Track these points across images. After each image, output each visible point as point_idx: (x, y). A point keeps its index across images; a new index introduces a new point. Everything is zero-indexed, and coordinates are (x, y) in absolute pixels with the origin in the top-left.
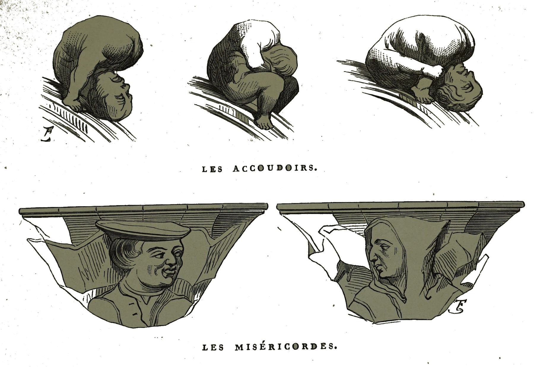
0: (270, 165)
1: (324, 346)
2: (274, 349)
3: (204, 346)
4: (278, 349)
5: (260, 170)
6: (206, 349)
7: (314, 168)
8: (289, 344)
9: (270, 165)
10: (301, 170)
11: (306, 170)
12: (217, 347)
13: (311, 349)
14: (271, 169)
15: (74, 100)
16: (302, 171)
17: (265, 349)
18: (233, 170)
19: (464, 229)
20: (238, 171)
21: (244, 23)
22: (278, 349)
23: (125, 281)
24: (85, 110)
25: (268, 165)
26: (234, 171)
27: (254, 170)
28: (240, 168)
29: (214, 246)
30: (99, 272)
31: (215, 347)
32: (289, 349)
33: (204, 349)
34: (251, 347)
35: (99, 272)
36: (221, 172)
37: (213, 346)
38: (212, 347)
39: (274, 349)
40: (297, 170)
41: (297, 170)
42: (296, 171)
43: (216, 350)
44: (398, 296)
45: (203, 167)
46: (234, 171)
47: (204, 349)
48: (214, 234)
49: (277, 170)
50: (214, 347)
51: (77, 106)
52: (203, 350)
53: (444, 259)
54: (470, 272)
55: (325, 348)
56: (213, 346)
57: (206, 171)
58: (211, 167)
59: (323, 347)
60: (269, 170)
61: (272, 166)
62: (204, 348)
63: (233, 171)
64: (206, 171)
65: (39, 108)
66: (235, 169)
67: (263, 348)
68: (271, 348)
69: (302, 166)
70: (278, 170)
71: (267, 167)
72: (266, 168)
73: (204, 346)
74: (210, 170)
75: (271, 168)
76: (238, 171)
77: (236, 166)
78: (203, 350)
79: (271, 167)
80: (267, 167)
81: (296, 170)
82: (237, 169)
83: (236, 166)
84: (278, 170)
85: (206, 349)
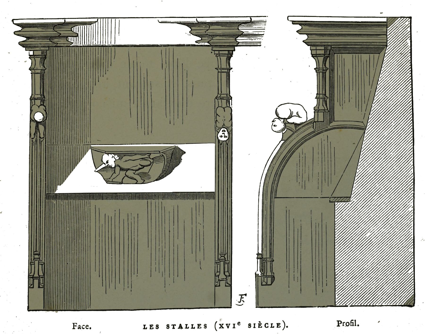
1: (260, 325)
3: (144, 325)
4: (233, 328)
6: (187, 327)
8: (268, 324)
12: (154, 327)
15: (108, 156)
17: (201, 328)
20: (227, 324)
21: (330, 199)
22: (233, 328)
24: (105, 157)
27: (268, 327)
31: (153, 326)
33: (144, 328)
34: (252, 326)
37: (199, 325)
43: (153, 328)
46: (229, 324)
47: (144, 328)
51: (150, 179)
52: (143, 329)
53: (159, 161)
54: (172, 171)
59: (260, 326)
62: (186, 326)
73: (144, 325)
78: (143, 329)
85: (187, 327)
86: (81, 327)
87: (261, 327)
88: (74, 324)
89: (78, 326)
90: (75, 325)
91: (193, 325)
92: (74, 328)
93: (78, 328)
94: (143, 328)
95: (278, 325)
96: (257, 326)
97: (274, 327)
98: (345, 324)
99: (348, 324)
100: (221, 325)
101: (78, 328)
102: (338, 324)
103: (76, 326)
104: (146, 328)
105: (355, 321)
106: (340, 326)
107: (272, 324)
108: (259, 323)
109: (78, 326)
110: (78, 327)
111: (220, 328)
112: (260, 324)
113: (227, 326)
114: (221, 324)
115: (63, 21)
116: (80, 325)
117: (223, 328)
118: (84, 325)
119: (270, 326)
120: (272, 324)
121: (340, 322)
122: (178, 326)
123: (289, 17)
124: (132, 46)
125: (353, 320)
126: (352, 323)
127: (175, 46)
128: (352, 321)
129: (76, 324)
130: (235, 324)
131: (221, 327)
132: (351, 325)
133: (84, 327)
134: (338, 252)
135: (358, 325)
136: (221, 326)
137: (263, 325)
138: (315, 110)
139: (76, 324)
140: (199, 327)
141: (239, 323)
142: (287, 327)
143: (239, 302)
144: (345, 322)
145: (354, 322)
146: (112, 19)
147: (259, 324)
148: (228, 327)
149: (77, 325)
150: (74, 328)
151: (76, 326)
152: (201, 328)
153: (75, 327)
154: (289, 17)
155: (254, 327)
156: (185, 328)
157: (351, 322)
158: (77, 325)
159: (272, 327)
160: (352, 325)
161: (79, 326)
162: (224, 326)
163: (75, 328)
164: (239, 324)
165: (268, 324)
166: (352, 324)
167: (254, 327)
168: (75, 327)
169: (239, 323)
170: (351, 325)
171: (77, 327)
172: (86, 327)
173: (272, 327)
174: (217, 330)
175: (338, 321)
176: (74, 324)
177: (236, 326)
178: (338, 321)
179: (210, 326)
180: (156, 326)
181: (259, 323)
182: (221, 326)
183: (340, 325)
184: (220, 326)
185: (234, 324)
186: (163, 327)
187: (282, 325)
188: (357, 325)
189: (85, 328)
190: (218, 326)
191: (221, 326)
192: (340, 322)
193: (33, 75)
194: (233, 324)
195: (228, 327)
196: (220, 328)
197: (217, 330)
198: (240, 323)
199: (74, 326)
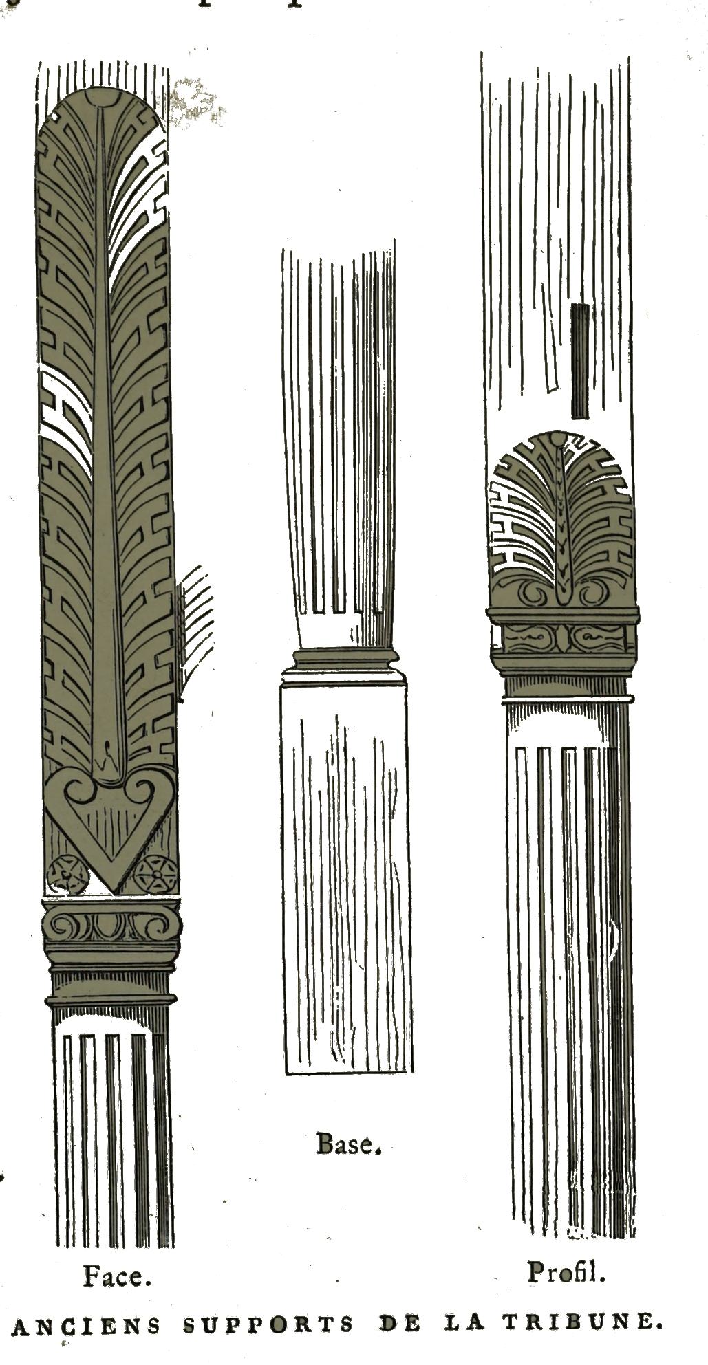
0: (595, 1315)
3: (450, 1317)
5: (277, 1329)
7: (653, 1321)
9: (595, 1315)
11: (310, 1331)
14: (210, 1327)
16: (87, 1336)
19: (112, 86)
20: (25, 1334)
23: (81, 781)
25: (202, 1319)
26: (14, 1334)
27: (73, 1333)
28: (31, 1327)
30: (352, 630)
33: (450, 1328)
34: (545, 1322)
35: (352, 630)
36: (348, 1331)
41: (513, 1328)
42: (87, 1336)
44: (344, 1028)
45: (551, 1315)
46: (14, 1334)
47: (450, 1328)
55: (114, 1332)
57: (457, 1328)
58: (639, 1314)
59: (644, 1322)
60: (593, 1326)
61: (602, 1315)
63: (468, 1329)
64: (457, 1328)
65: (124, 1247)
66: (472, 1323)
69: (529, 1316)
70: (384, 1328)
71: (202, 1324)
72: (585, 1321)
75: (597, 1323)
76: (25, 1334)
77: (475, 1316)
79: (210, 1324)
80: (589, 1318)
82: (22, 1328)
83: (475, 1316)
84: (384, 1328)
85: (454, 1326)
86: (114, 1281)
88: (88, 1268)
89: (104, 1277)
90: (93, 1271)
92: (88, 1284)
93: (104, 1284)
94: (84, 1331)
98: (556, 1276)
99: (566, 1276)
101: (104, 1284)
103: (96, 1275)
105: (592, 1262)
109: (104, 1277)
110: (103, 1279)
114: (21, 1335)
116: (110, 1274)
117: (482, 1328)
118: (124, 1274)
121: (256, 1322)
123: (290, 1071)
125: (583, 1262)
126: (580, 1270)
128: (581, 1266)
129: (98, 1267)
130: (85, 1285)
132: (577, 1280)
133: (122, 1279)
134: (614, 118)
135: (603, 1280)
139: (98, 1267)
142: (659, 1326)
143: (165, 930)
144: (555, 1270)
145: (588, 1267)
149: (101, 1273)
150: (88, 1284)
151: (96, 1275)
152: (114, 1332)
153: (92, 1278)
154: (290, 1071)
155: (554, 1328)
157: (577, 1269)
158: (101, 1273)
160: (581, 1277)
161: (107, 1277)
163: (91, 1283)
166: (581, 1274)
168: (93, 1280)
170: (577, 1280)
171: (100, 1280)
172: (132, 1278)
176: (88, 1268)
183: (256, 1328)
188: (597, 1277)
189: (129, 1284)
192: (233, 1322)
194: (91, 1334)
199: (88, 1275)
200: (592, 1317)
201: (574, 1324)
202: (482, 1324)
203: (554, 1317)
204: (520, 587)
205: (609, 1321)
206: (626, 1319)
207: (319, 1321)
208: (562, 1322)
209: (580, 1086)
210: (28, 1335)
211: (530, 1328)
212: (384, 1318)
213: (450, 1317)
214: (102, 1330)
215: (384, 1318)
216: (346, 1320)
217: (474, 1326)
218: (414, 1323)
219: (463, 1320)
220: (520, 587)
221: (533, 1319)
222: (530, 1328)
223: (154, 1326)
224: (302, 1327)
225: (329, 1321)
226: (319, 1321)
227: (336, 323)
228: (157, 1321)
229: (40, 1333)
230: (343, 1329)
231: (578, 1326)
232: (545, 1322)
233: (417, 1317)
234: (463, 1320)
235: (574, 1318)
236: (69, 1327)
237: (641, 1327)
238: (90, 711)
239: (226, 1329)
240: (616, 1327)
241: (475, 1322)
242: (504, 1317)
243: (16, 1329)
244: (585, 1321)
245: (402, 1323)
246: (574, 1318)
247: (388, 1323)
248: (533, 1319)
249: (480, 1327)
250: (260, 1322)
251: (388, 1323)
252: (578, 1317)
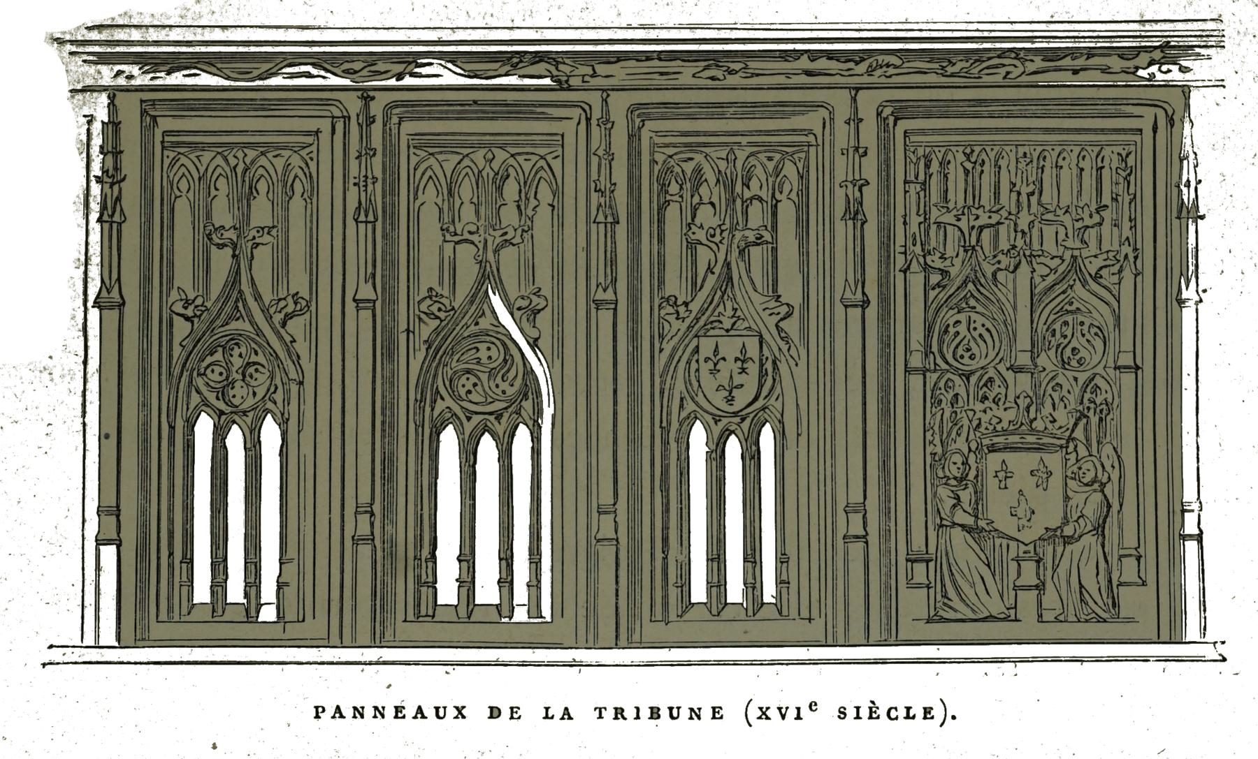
2: (625, 719)
3: (547, 709)
6: (911, 715)
8: (896, 709)
10: (795, 719)
13: (905, 718)
17: (519, 718)
18: (414, 715)
20: (342, 716)
26: (334, 717)
27: (896, 718)
29: (472, 611)
32: (896, 718)
33: (547, 717)
34: (851, 713)
36: (844, 718)
38: (714, 712)
39: (625, 719)
40: (861, 718)
47: (547, 717)
48: (97, 636)
49: (489, 718)
50: (516, 712)
52: (544, 718)
55: (404, 717)
56: (515, 710)
57: (552, 717)
60: (672, 717)
61: (678, 708)
64: (552, 717)
67: (400, 715)
68: (619, 716)
69: (616, 709)
70: (491, 717)
71: (668, 711)
72: (664, 713)
74: (920, 714)
76: (342, 716)
78: (544, 718)
81: (858, 717)
82: (422, 713)
83: (566, 709)
84: (491, 717)
85: (911, 715)
87: (878, 717)
91: (911, 708)
94: (544, 715)
95: (927, 711)
96: (864, 713)
97: (914, 717)
100: (764, 710)
102: (317, 712)
104: (914, 717)
106: (320, 718)
107: (908, 709)
108: (872, 705)
111: (760, 718)
112: (398, 710)
113: (569, 714)
115: (1189, 494)
117: (572, 719)
119: (902, 713)
120: (908, 709)
121: (320, 710)
122: (330, 711)
124: (119, 628)
127: (120, 624)
131: (764, 717)
136: (764, 713)
137: (882, 712)
138: (461, 582)
140: (400, 715)
141: (812, 706)
142: (954, 717)
146: (274, 607)
147: (870, 708)
148: (783, 717)
156: (905, 718)
159: (908, 717)
162: (773, 713)
164: (814, 708)
165: (896, 709)
167: (858, 717)
169: (812, 706)
173: (908, 717)
174: (750, 725)
175: (317, 708)
177: (805, 712)
178: (317, 708)
179: (733, 713)
180: (840, 712)
181: (872, 705)
182: (764, 713)
183: (320, 714)
184: (760, 713)
185: (798, 709)
186: (532, 713)
187: (938, 712)
190: (754, 713)
191: (764, 714)
192: (320, 710)
193: (710, 562)
195: (783, 717)
196: (760, 718)
197: (750, 725)
198: (816, 704)
200: (671, 709)
201: (655, 716)
202: (572, 716)
203: (858, 708)
204: (1056, 352)
205: (685, 713)
206: (355, 714)
207: (553, 716)
208: (645, 713)
209: (161, 534)
210: (344, 717)
211: (616, 718)
212: (491, 708)
213: (547, 709)
214: (394, 714)
215: (491, 708)
216: (842, 710)
217: (460, 716)
218: (401, 712)
219: (557, 711)
220: (1056, 352)
221: (619, 711)
222: (616, 718)
223: (716, 712)
224: (619, 716)
225: (603, 710)
226: (553, 716)
227: (261, 100)
228: (845, 709)
229: (355, 717)
230: (839, 717)
231: (659, 717)
232: (630, 713)
233: (932, 708)
234: (557, 711)
235: (655, 710)
236: (893, 714)
237: (396, 717)
238: (765, 347)
239: (315, 715)
240: (691, 718)
241: (567, 715)
242: (595, 709)
243: (417, 713)
244: (664, 713)
245: (506, 713)
246: (655, 710)
247: (494, 713)
248: (619, 711)
249: (570, 718)
250: (324, 710)
251: (494, 713)
252: (659, 709)
